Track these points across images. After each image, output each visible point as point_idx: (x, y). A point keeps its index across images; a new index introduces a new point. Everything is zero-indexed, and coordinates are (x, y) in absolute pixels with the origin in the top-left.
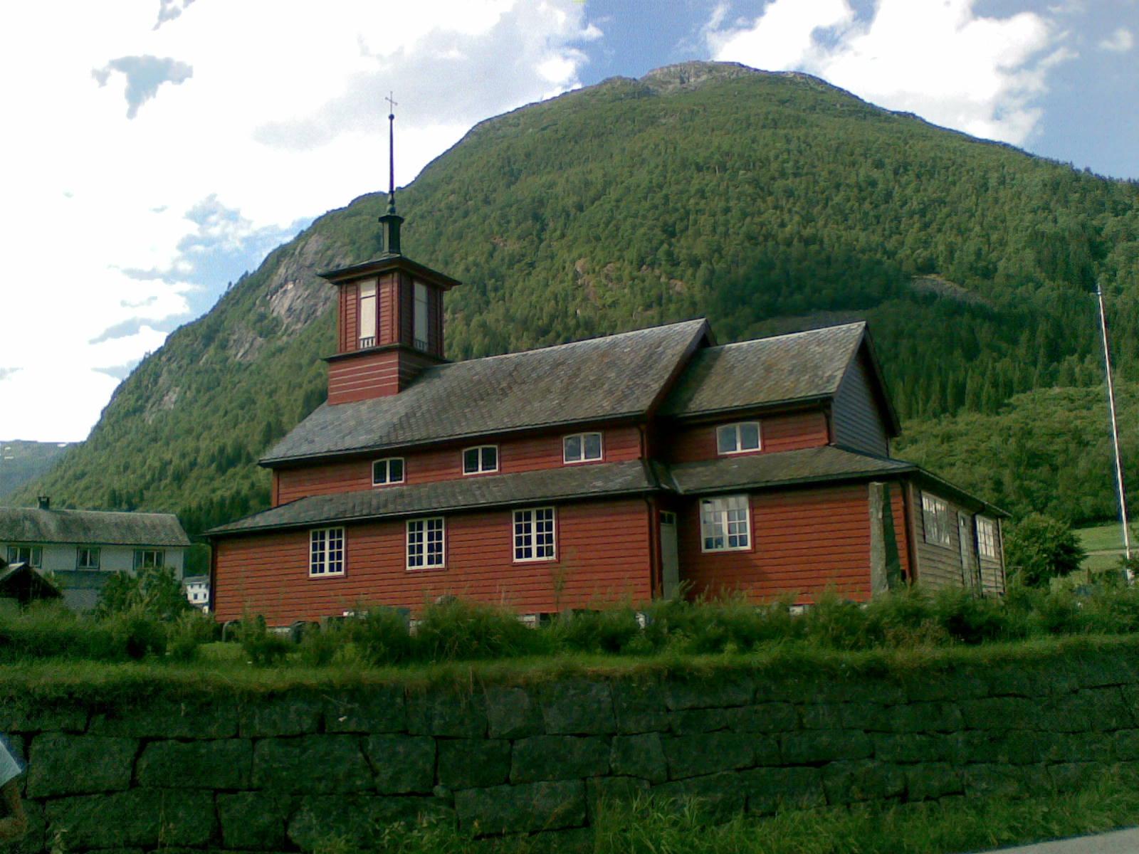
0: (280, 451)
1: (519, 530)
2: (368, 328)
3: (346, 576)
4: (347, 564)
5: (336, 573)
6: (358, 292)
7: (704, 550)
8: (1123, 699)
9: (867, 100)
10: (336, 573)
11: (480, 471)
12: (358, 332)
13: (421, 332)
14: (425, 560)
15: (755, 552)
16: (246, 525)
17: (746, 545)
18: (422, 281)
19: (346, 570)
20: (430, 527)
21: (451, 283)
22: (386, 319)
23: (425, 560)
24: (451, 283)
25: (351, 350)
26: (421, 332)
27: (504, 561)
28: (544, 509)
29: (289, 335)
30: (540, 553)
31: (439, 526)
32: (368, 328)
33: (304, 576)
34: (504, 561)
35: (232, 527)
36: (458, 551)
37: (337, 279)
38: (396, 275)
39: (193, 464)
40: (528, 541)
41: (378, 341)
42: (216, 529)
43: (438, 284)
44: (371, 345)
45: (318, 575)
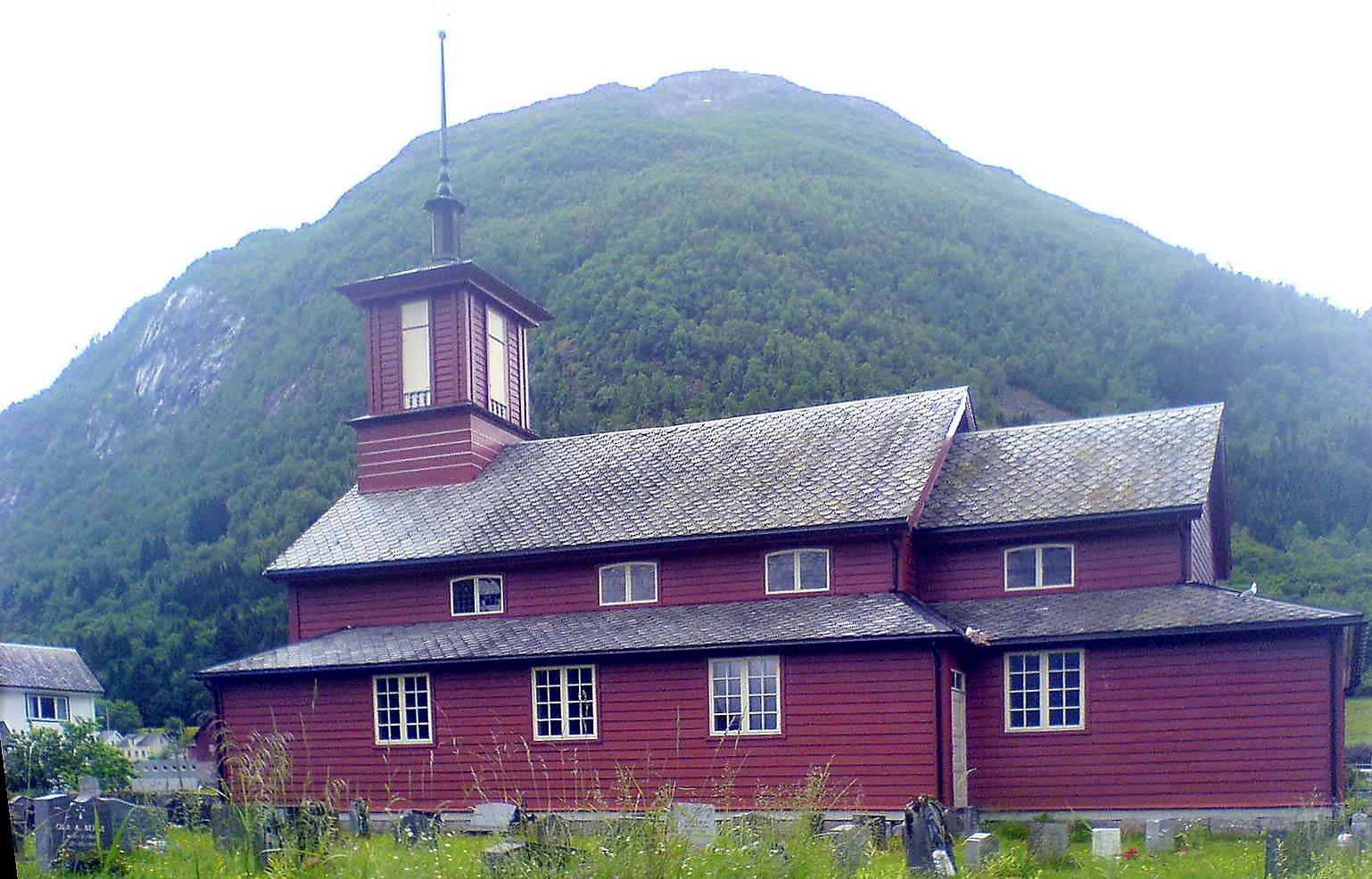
0: (296, 557)
1: (542, 694)
4: (435, 727)
5: (418, 741)
7: (1009, 728)
8: (27, 859)
9: (952, 146)
10: (418, 741)
15: (601, 743)
16: (267, 666)
17: (1077, 722)
19: (601, 731)
20: (409, 686)
27: (364, 744)
28: (579, 667)
29: (164, 423)
30: (574, 728)
31: (422, 686)
34: (364, 744)
35: (243, 665)
39: (48, 591)
40: (556, 711)
41: (436, 398)
42: (218, 668)
44: (425, 402)
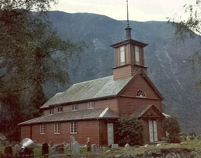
2: (123, 59)
3: (77, 134)
6: (120, 50)
11: (60, 112)
12: (120, 61)
13: (137, 59)
14: (74, 131)
18: (138, 45)
21: (145, 45)
22: (127, 58)
23: (74, 131)
24: (145, 45)
25: (119, 66)
26: (137, 59)
32: (123, 59)
33: (39, 133)
36: (80, 129)
37: (114, 47)
38: (129, 44)
41: (126, 63)
43: (142, 46)
45: (72, 133)
